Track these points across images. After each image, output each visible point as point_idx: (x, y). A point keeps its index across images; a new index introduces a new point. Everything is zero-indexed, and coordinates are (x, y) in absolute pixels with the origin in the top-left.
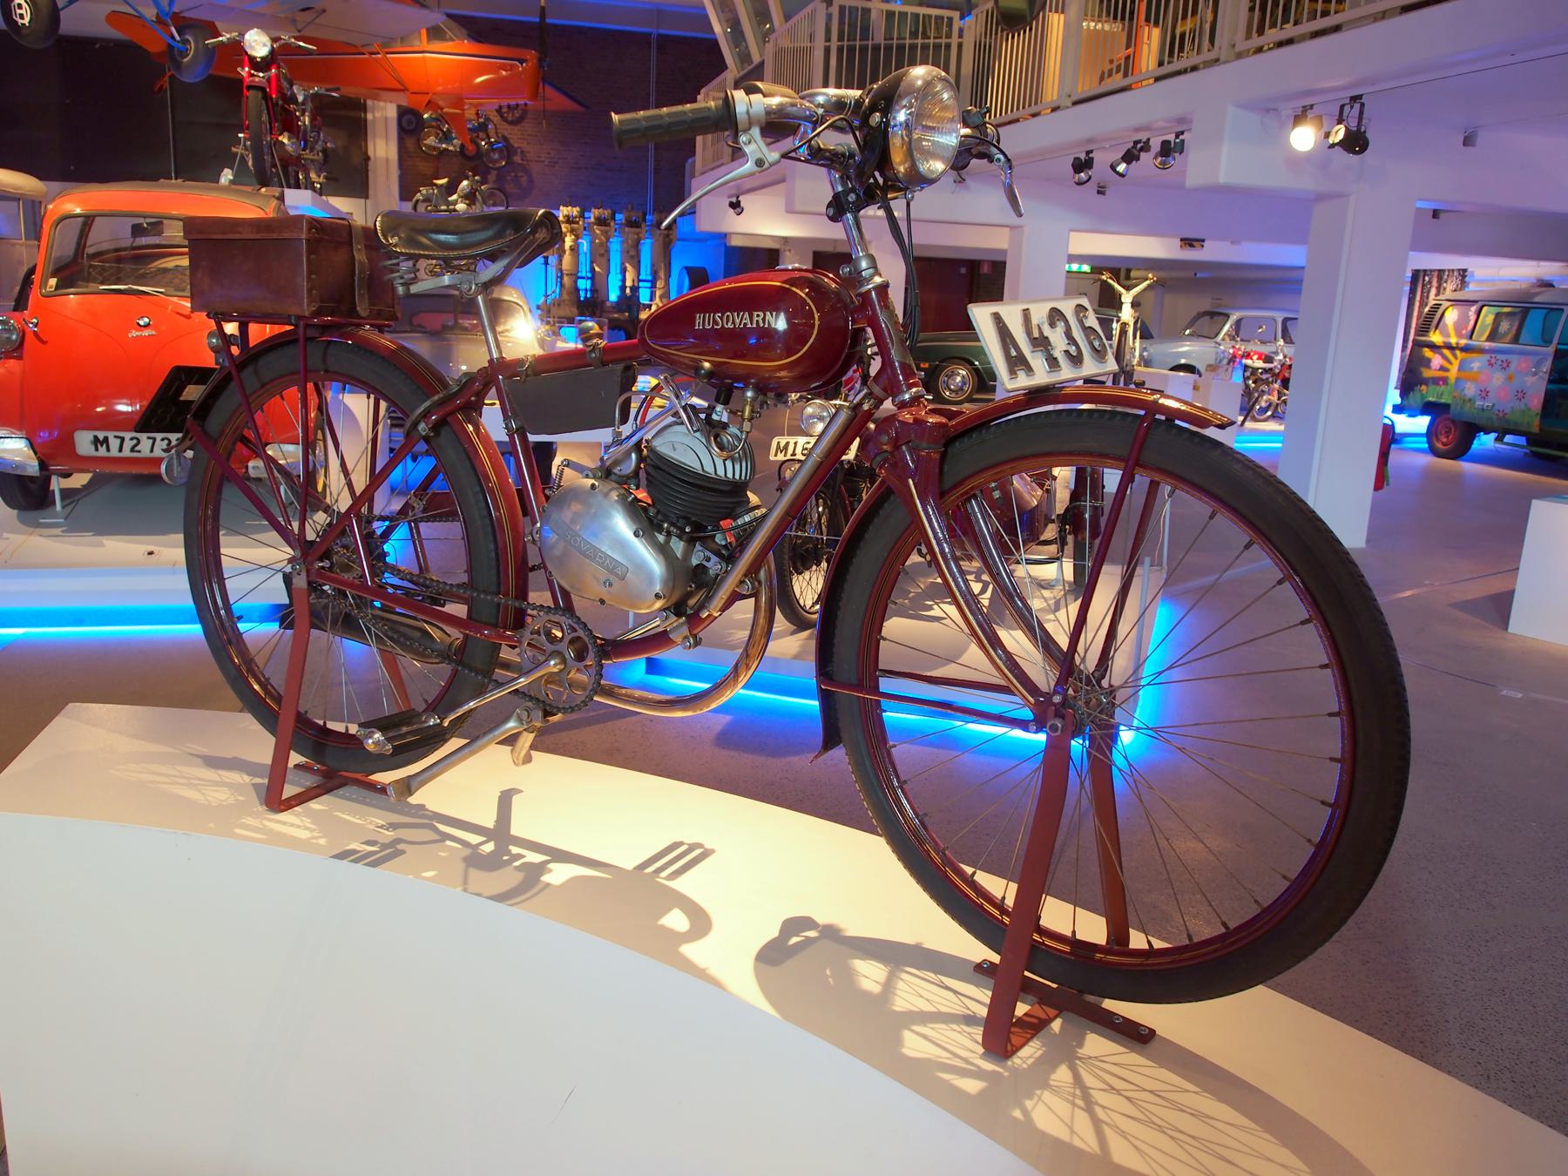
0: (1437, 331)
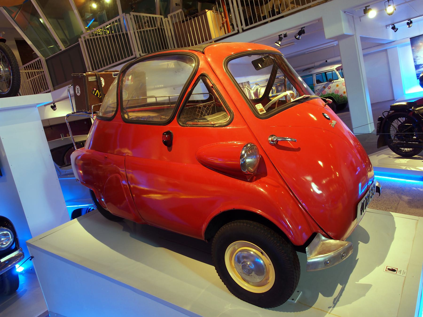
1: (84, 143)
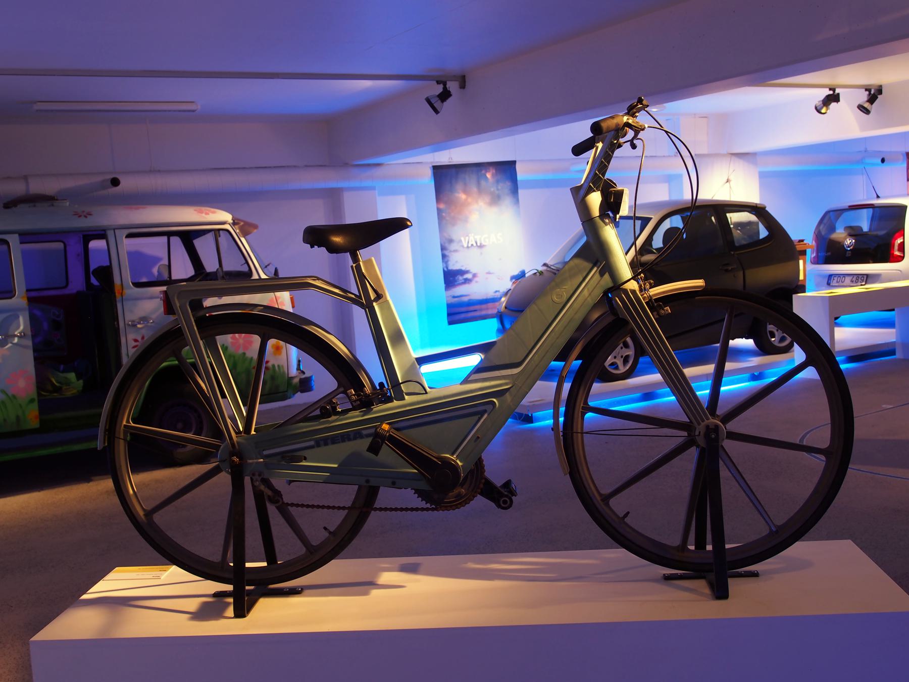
1: (467, 282)
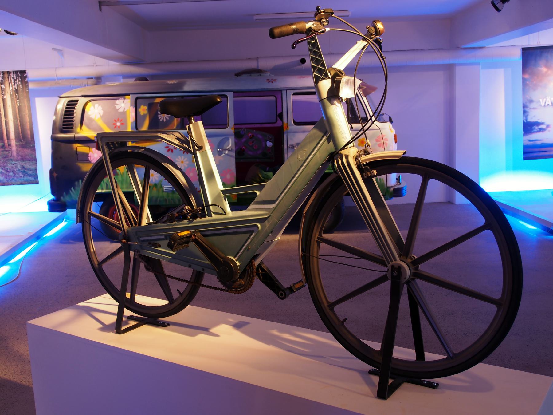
0: (84, 126)
1: (542, 130)
